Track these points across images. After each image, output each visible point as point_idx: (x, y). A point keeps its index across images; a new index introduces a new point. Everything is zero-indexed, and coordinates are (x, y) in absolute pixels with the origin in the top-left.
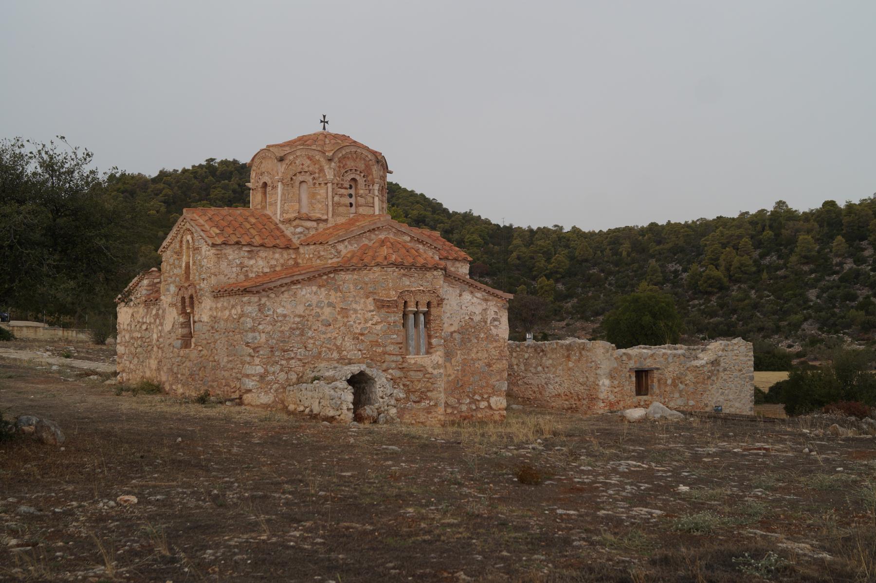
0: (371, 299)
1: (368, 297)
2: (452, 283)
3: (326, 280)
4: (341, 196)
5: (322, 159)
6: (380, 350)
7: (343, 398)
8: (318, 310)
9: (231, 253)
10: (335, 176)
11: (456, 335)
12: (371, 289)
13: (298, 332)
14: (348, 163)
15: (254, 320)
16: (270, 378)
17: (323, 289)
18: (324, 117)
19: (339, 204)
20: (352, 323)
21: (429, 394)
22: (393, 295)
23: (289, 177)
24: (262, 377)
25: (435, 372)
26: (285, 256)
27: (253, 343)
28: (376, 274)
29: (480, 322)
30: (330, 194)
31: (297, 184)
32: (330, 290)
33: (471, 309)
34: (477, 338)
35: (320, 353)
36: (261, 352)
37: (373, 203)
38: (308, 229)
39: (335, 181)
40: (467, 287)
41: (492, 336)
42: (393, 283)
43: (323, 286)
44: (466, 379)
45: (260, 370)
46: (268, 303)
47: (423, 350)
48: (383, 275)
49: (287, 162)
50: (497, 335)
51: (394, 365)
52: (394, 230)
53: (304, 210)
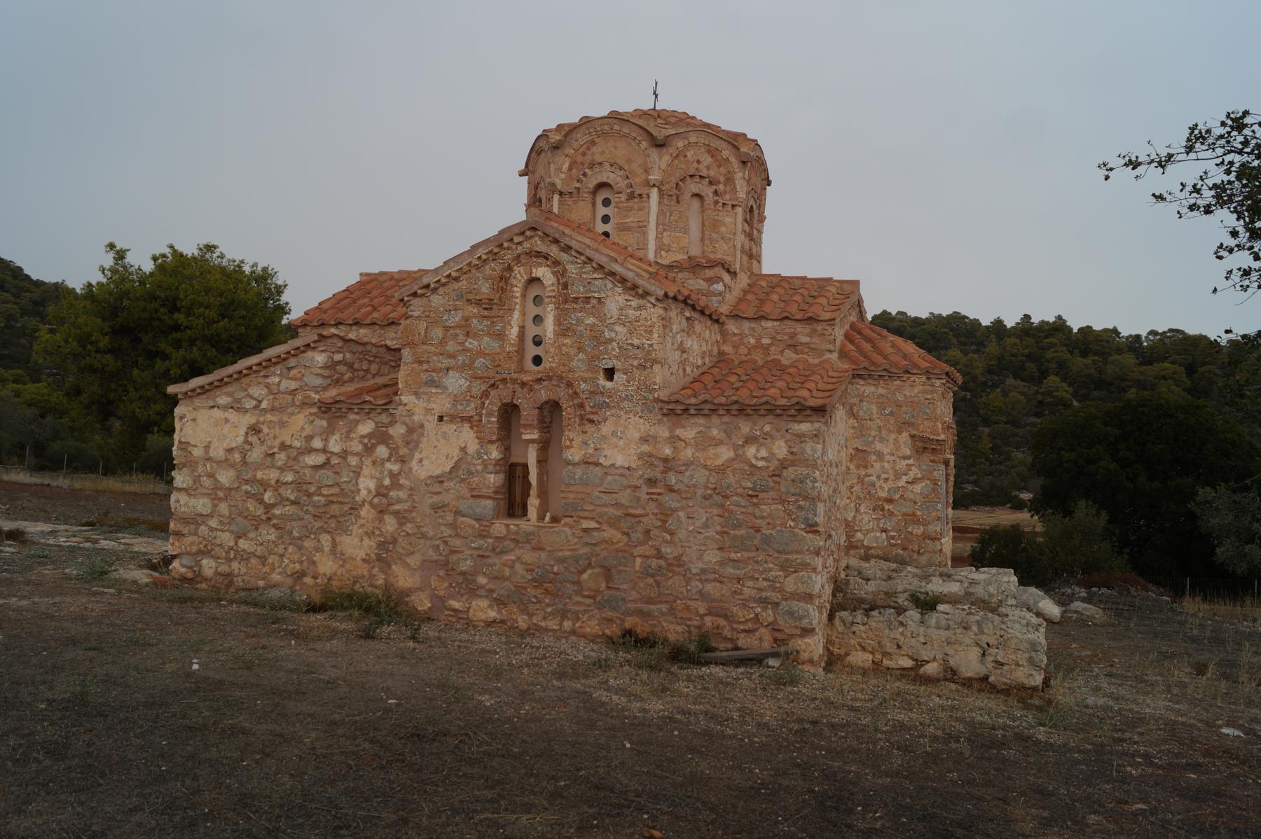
0: (905, 435)
1: (900, 432)
5: (733, 159)
6: (918, 530)
20: (874, 478)
23: (674, 180)
48: (926, 392)
49: (672, 150)
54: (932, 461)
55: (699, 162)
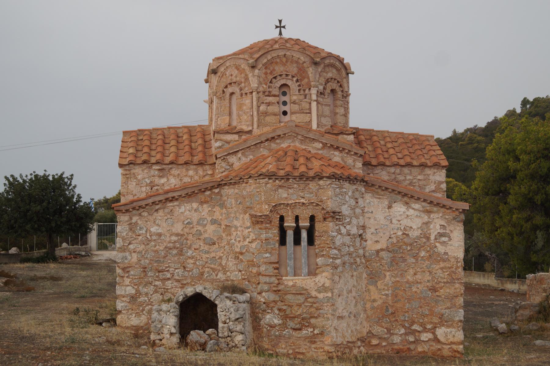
1: (245, 213)
2: (377, 193)
3: (209, 196)
4: (269, 104)
6: (255, 270)
7: (163, 321)
8: (200, 228)
9: (140, 172)
10: (260, 83)
11: (383, 254)
12: (248, 204)
13: (175, 252)
14: (277, 68)
15: (124, 239)
16: (141, 299)
17: (205, 206)
18: (280, 21)
19: (266, 114)
20: (233, 241)
21: (313, 321)
22: (266, 209)
23: (221, 89)
24: (133, 298)
25: (321, 296)
26: (201, 172)
27: (123, 263)
28: (250, 187)
29: (419, 238)
30: (255, 103)
31: (228, 95)
32: (214, 207)
33: (406, 222)
34: (416, 257)
35: (202, 274)
36: (132, 273)
37: (310, 109)
38: (228, 143)
39: (261, 89)
40: (399, 197)
41: (439, 254)
42: (262, 195)
43: (206, 202)
44: (399, 305)
45: (130, 290)
46: (139, 222)
47: (305, 270)
48: (257, 188)
50: (446, 253)
51: (266, 287)
52: (300, 137)
53: (234, 123)
54: (260, 229)
55: (232, 75)
